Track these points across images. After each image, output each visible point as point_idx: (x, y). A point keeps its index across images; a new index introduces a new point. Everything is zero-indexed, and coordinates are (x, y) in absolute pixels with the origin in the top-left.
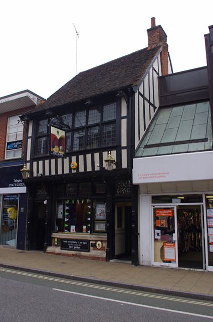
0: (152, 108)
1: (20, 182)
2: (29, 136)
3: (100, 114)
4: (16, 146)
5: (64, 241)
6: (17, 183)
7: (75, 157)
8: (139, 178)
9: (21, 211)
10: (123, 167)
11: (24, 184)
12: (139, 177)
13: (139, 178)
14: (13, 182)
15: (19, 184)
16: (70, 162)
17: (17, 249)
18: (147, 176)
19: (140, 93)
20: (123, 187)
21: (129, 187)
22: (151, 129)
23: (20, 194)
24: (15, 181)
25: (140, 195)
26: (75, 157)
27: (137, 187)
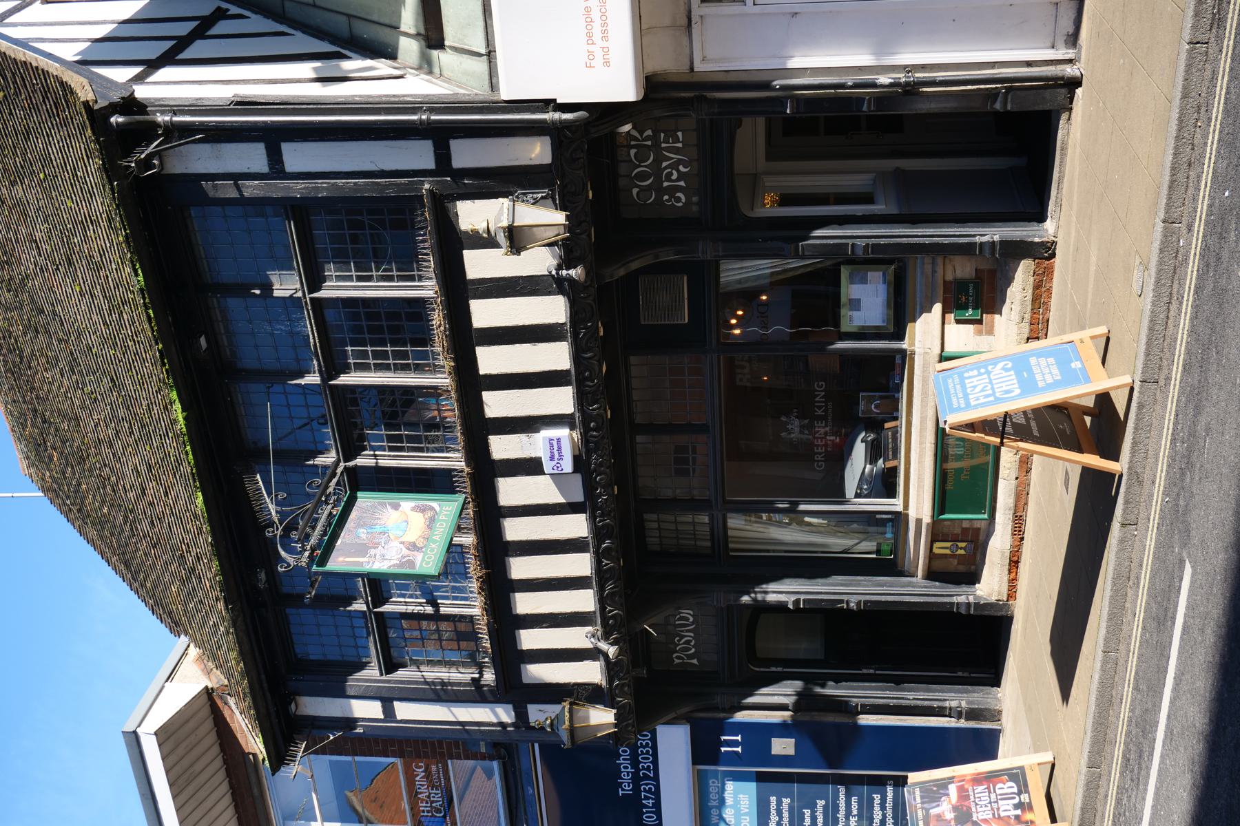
0: (221, 27)
1: (635, 762)
2: (398, 705)
3: (454, 547)
4: (437, 795)
5: (878, 516)
6: (636, 779)
7: (434, 168)
8: (607, 63)
9: (791, 751)
10: (547, 159)
11: (645, 740)
12: (598, 61)
13: (607, 63)
14: (634, 801)
15: (645, 763)
16: (485, 241)
17: (1022, 768)
18: (596, 15)
19: (139, 79)
20: (657, 170)
21: (655, 137)
22: (340, 24)
23: (695, 761)
24: (626, 788)
25: (699, 66)
26: (434, 168)
27: (652, 84)
